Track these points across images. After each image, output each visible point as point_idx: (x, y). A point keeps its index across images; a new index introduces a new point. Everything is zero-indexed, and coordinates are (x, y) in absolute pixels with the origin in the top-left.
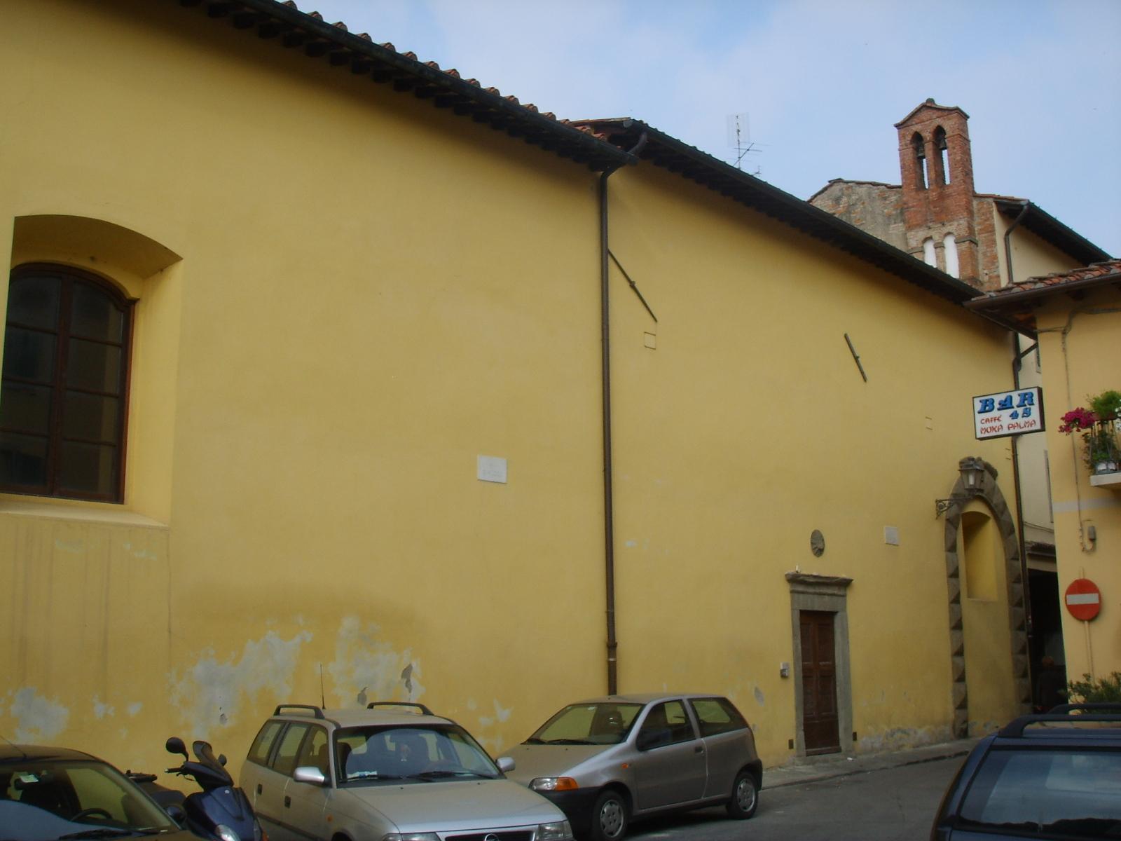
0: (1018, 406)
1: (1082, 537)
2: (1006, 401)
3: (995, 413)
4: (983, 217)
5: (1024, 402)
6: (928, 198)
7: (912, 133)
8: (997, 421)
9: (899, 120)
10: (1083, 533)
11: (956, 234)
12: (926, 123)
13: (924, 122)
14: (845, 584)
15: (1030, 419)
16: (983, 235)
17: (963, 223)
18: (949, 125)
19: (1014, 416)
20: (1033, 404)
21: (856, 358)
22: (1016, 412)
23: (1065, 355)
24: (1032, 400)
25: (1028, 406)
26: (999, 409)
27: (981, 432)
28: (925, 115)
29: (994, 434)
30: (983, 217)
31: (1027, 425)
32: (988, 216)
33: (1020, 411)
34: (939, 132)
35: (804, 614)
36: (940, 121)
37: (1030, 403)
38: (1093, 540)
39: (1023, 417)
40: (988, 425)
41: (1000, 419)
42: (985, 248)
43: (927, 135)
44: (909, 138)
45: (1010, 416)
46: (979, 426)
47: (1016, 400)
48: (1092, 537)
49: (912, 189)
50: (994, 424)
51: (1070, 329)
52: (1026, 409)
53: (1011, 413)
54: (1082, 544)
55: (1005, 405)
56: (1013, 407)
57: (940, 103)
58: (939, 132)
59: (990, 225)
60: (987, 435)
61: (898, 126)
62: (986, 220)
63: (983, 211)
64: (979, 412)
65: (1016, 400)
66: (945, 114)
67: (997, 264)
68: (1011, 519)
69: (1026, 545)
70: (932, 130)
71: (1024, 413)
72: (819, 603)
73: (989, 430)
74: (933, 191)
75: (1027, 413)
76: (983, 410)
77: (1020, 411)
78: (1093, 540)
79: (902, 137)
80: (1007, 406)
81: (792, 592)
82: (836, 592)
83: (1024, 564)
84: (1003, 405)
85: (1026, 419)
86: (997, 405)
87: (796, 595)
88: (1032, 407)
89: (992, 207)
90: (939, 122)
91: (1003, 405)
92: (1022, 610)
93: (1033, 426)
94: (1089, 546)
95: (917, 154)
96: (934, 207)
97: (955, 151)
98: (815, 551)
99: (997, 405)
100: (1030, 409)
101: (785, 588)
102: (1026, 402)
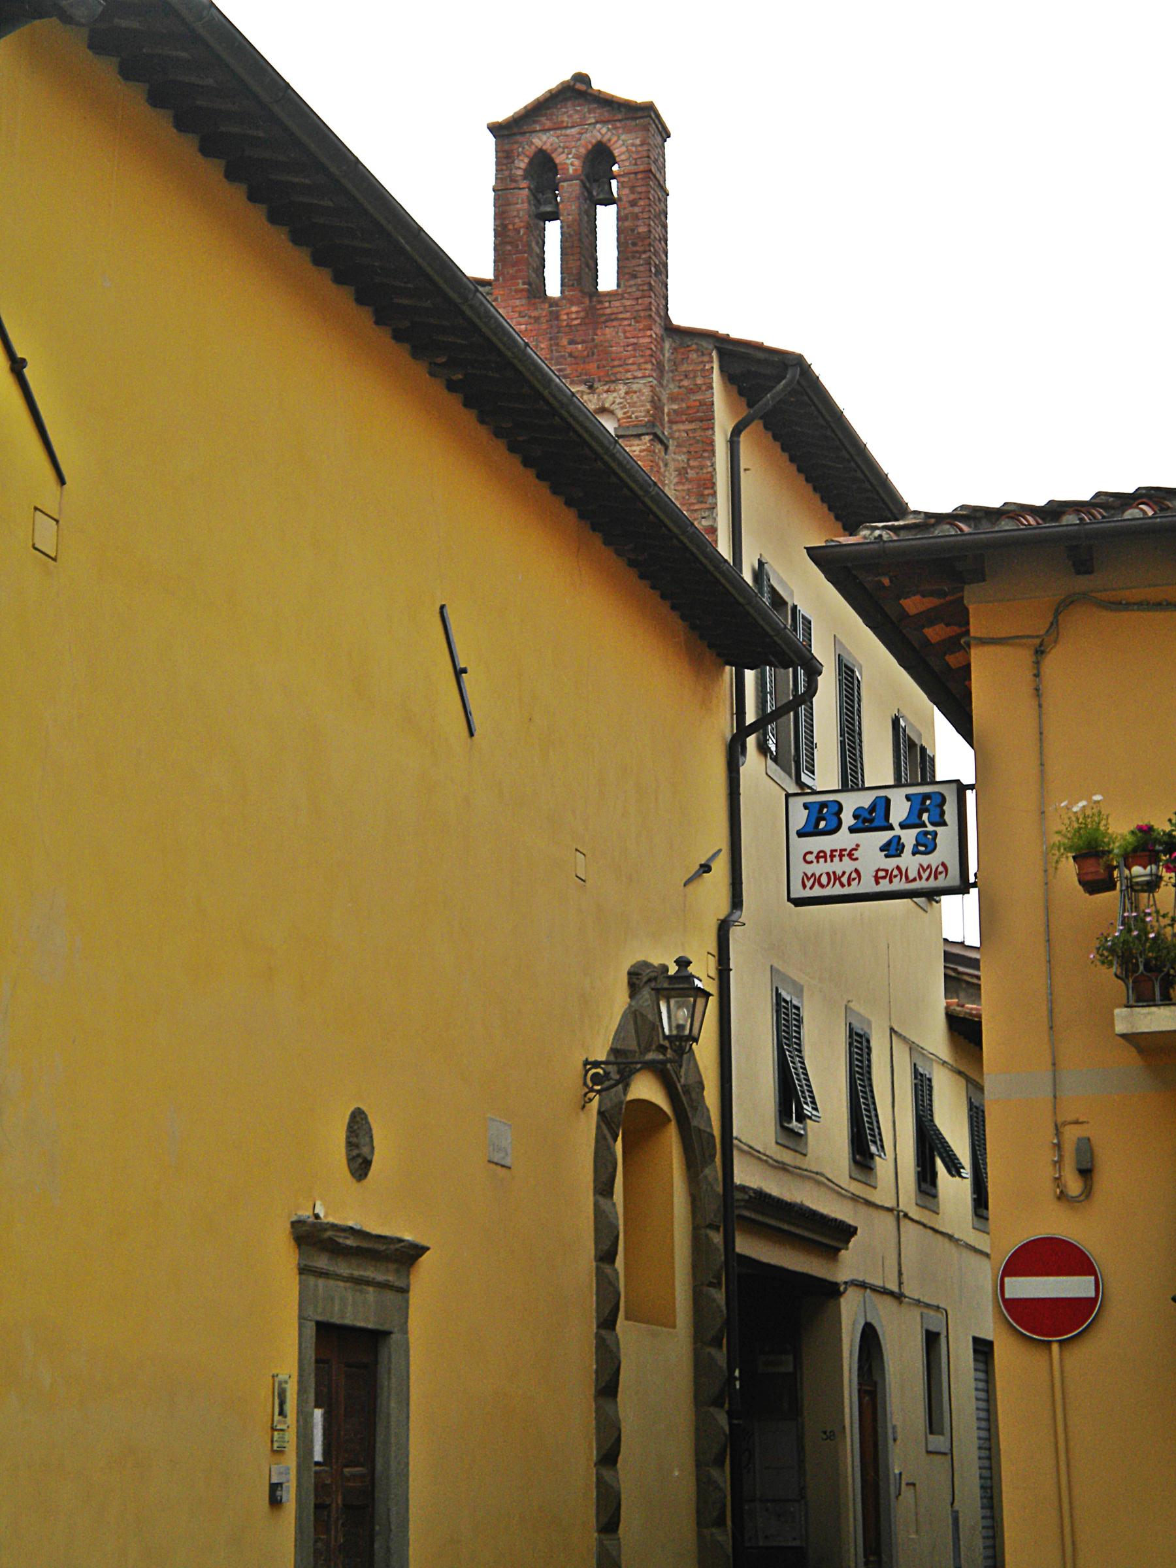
0: (903, 826)
1: (1058, 1164)
2: (873, 808)
3: (843, 839)
4: (686, 383)
5: (920, 816)
6: (557, 318)
7: (531, 151)
8: (846, 859)
9: (502, 114)
10: (1061, 1156)
11: (620, 414)
12: (568, 131)
13: (566, 128)
14: (408, 1255)
15: (933, 860)
16: (682, 427)
17: (643, 387)
18: (623, 144)
19: (893, 849)
20: (944, 824)
21: (459, 672)
22: (899, 838)
23: (1040, 706)
24: (943, 813)
25: (930, 828)
26: (852, 830)
27: (804, 886)
28: (569, 113)
29: (837, 890)
30: (686, 383)
31: (925, 876)
32: (699, 381)
33: (909, 837)
34: (600, 157)
35: (323, 1329)
36: (604, 130)
37: (937, 819)
38: (1086, 1173)
39: (914, 854)
40: (821, 868)
41: (856, 854)
42: (684, 457)
43: (570, 162)
44: (522, 163)
45: (882, 850)
46: (799, 868)
47: (900, 810)
48: (1085, 1166)
49: (517, 291)
50: (837, 866)
51: (1056, 642)
52: (926, 833)
53: (887, 839)
54: (1057, 1180)
55: (871, 821)
56: (891, 828)
57: (599, 84)
58: (600, 157)
59: (702, 403)
60: (817, 892)
61: (495, 129)
62: (691, 391)
63: (685, 367)
64: (800, 834)
65: (900, 810)
66: (620, 117)
67: (710, 500)
68: (711, 1126)
69: (738, 1195)
70: (583, 151)
71: (918, 844)
72: (356, 1310)
73: (824, 880)
74: (572, 303)
75: (926, 845)
76: (810, 829)
77: (909, 837)
78: (1086, 1173)
79: (504, 159)
80: (875, 824)
81: (303, 1270)
82: (391, 1278)
83: (729, 1242)
84: (865, 820)
85: (925, 860)
86: (847, 819)
87: (312, 1280)
88: (939, 829)
89: (712, 362)
90: (601, 132)
91: (865, 820)
92: (721, 1357)
93: (855, 883)
94: (1074, 1186)
95: (537, 208)
96: (571, 342)
97: (637, 210)
98: (356, 1165)
99: (847, 819)
100: (935, 834)
101: (283, 1258)
102: (925, 817)
